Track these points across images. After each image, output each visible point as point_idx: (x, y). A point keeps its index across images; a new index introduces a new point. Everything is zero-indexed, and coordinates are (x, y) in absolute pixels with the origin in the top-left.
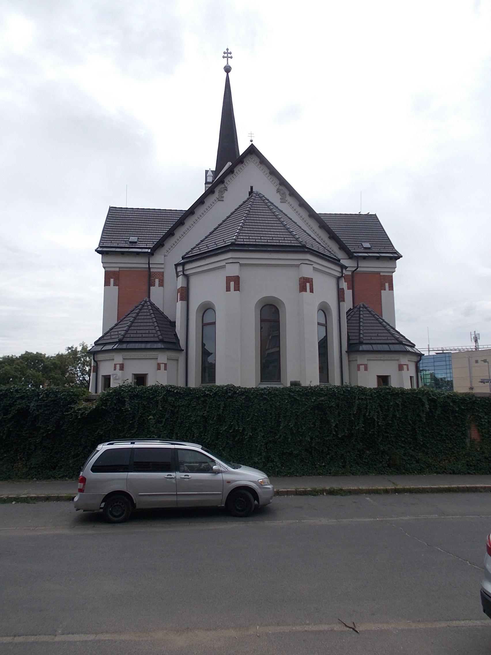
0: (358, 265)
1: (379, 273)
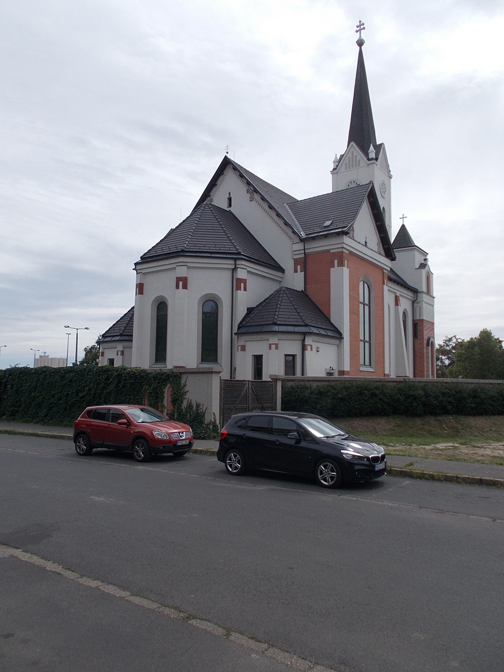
0: (304, 247)
1: (328, 251)
